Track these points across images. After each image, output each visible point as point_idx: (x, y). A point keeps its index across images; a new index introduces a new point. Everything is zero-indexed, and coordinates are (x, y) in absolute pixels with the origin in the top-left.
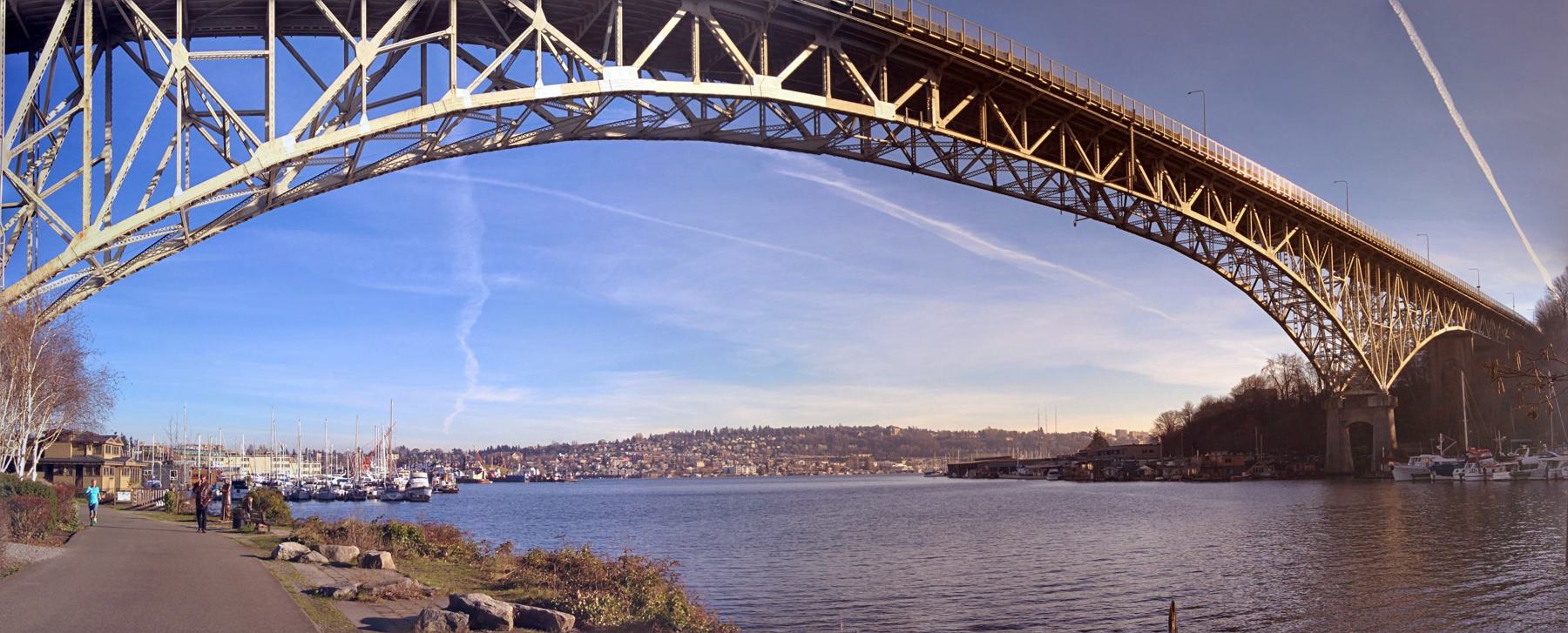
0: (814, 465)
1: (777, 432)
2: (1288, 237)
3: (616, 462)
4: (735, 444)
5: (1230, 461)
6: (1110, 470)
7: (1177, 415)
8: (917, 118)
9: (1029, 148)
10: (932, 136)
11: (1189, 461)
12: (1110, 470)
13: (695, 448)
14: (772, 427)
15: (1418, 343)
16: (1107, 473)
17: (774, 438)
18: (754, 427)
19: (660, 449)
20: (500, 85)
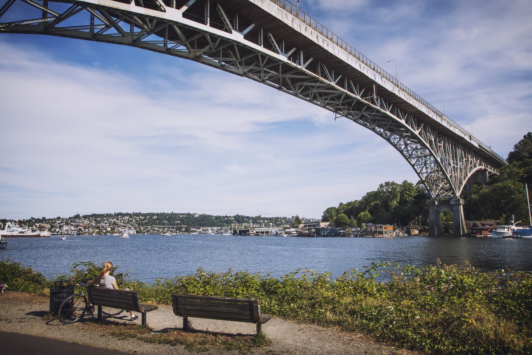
0: (162, 230)
1: (145, 215)
3: (65, 228)
4: (125, 220)
5: (386, 228)
6: (324, 233)
7: (18, 290)
8: (295, 63)
9: (335, 81)
10: (61, 25)
12: (324, 233)
13: (105, 222)
14: (142, 212)
15: (468, 174)
16: (322, 234)
17: (143, 218)
18: (134, 212)
19: (88, 222)
20: (142, 17)
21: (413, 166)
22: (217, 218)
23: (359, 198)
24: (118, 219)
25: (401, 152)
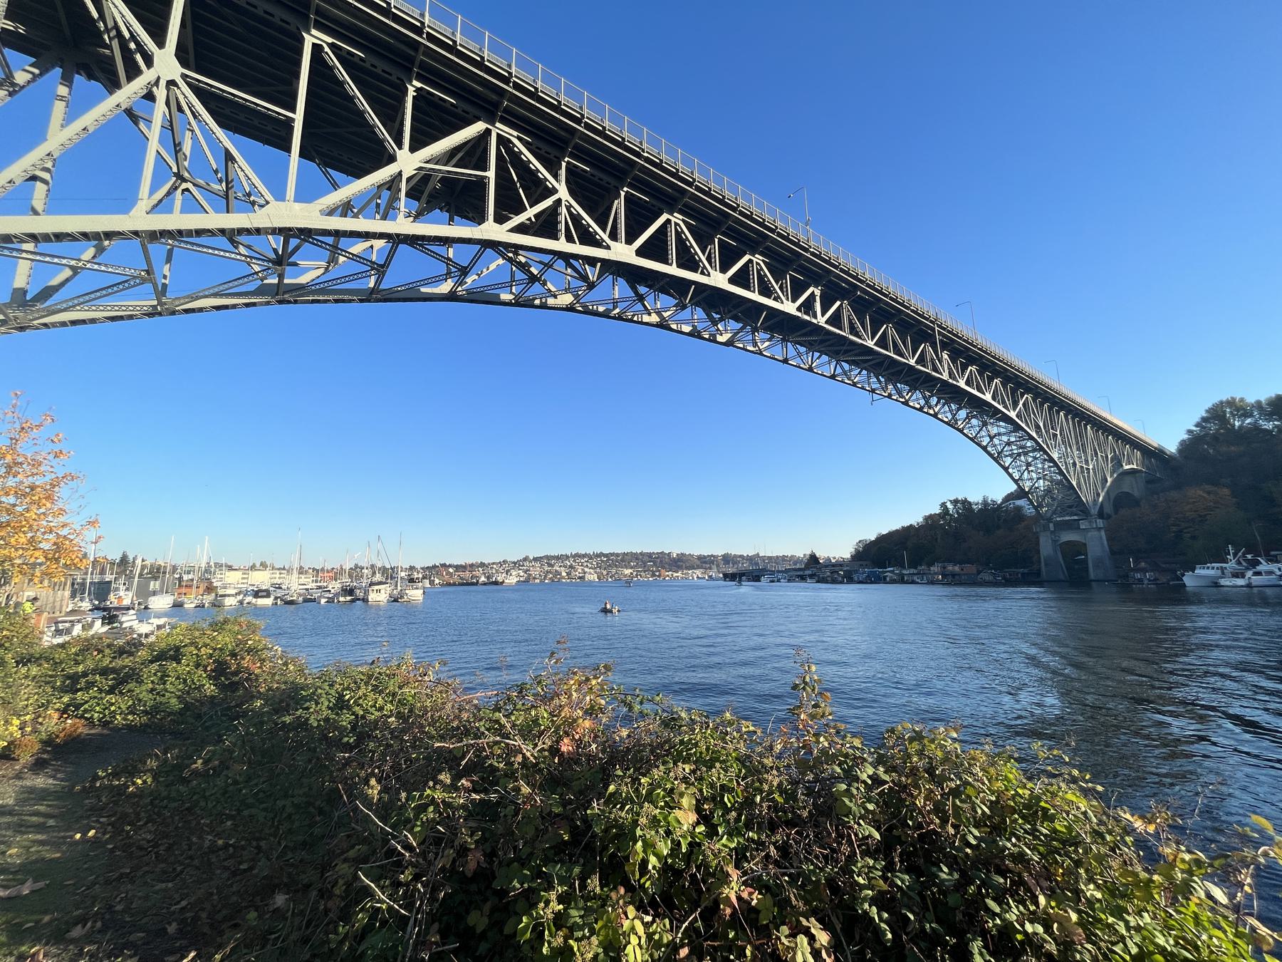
2: (1021, 402)
11: (944, 568)
21: (1006, 469)
22: (700, 558)
23: (873, 539)
24: (574, 561)
25: (984, 448)
